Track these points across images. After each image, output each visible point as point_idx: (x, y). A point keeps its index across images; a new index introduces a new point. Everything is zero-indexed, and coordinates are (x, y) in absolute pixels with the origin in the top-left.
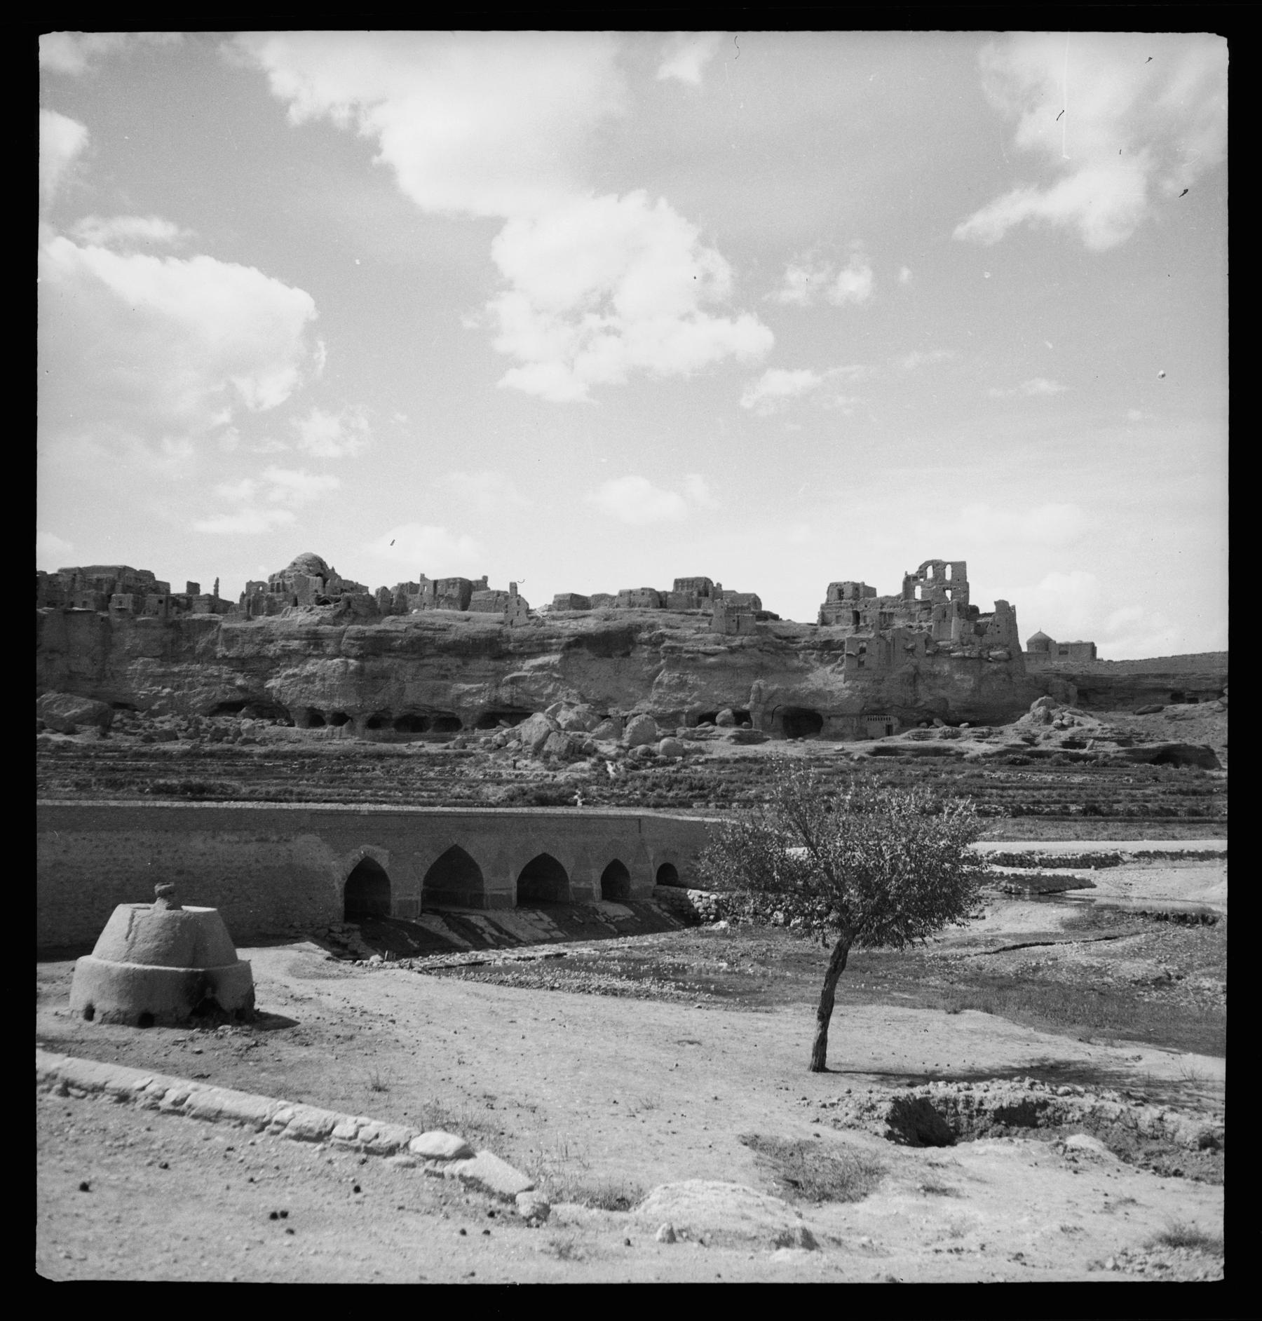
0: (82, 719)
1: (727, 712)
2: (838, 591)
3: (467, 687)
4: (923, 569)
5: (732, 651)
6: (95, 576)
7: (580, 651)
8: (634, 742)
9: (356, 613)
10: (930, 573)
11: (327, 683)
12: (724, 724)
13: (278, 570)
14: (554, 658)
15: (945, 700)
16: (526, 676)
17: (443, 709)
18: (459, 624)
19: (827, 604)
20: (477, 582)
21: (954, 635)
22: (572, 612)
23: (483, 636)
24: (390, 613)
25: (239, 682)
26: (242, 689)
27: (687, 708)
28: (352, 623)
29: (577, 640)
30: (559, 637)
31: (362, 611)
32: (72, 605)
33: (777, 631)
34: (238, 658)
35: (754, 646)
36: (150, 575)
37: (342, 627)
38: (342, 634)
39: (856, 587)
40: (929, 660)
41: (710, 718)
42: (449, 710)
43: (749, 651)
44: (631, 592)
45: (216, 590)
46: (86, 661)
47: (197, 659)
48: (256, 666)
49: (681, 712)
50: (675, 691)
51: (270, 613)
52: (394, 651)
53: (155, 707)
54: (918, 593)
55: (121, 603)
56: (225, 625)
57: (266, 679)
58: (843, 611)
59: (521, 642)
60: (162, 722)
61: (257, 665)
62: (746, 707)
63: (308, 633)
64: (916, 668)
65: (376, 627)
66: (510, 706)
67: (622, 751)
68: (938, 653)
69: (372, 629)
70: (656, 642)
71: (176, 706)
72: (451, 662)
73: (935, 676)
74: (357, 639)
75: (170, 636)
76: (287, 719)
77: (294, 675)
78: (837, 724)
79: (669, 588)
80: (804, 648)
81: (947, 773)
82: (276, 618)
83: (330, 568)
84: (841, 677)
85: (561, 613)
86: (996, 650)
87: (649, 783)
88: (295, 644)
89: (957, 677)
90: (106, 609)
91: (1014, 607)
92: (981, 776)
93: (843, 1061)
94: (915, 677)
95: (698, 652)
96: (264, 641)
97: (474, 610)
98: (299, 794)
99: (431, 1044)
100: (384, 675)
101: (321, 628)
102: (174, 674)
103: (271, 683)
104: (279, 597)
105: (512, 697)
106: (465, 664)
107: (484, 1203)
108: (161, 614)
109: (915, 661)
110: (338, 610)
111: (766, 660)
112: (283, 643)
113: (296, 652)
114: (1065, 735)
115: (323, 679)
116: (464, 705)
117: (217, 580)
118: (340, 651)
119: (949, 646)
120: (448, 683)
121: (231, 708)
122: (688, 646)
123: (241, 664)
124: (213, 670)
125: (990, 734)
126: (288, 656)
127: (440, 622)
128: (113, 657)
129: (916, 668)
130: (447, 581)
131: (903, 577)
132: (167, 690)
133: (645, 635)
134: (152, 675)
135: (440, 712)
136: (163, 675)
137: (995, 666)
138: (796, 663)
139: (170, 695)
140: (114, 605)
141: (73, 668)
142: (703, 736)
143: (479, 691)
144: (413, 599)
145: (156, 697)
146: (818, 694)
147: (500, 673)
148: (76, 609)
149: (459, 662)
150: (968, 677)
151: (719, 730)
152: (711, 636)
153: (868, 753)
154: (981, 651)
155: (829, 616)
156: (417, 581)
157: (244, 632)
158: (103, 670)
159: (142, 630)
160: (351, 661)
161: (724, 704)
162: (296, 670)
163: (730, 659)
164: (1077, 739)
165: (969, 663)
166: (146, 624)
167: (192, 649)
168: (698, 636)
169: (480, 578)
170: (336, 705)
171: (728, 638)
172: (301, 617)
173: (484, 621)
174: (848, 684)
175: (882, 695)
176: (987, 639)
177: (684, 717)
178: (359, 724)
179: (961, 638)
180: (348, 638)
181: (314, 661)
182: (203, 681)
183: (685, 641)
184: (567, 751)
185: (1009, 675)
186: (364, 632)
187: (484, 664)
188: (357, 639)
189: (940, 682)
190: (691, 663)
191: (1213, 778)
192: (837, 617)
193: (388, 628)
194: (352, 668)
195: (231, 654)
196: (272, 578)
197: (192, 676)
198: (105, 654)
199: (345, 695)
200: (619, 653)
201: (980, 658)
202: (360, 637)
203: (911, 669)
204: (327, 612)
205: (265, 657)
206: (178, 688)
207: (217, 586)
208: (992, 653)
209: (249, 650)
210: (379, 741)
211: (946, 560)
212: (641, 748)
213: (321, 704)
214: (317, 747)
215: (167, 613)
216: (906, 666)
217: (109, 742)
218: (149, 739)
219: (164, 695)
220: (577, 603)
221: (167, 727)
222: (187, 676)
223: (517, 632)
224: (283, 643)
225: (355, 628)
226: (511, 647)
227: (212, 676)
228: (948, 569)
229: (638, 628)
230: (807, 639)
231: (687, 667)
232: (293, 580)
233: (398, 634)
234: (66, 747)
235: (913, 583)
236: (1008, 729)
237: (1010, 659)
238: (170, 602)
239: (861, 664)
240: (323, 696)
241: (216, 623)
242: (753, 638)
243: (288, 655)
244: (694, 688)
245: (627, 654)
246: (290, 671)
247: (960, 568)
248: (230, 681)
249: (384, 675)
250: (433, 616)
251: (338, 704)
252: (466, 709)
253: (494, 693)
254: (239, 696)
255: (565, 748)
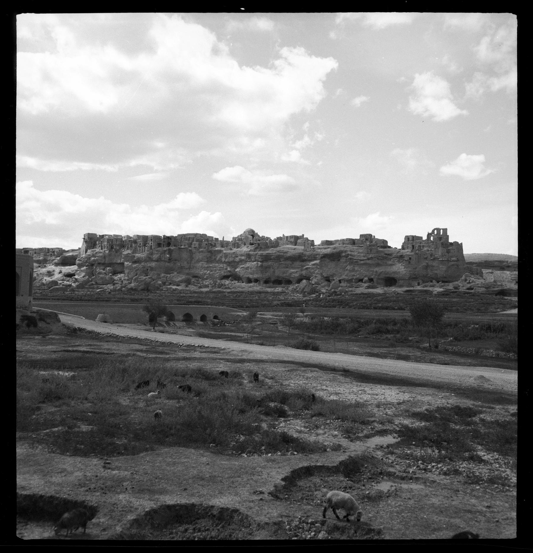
0: (181, 282)
1: (366, 279)
2: (407, 238)
3: (293, 271)
4: (433, 231)
5: (368, 259)
7: (325, 259)
8: (332, 289)
9: (261, 248)
10: (436, 232)
11: (252, 270)
12: (365, 282)
13: (239, 234)
14: (317, 262)
15: (436, 274)
16: (310, 267)
17: (287, 278)
20: (300, 236)
21: (440, 253)
22: (326, 246)
23: (297, 255)
25: (229, 269)
27: (355, 277)
28: (260, 251)
30: (319, 255)
31: (263, 247)
32: (181, 246)
33: (386, 252)
34: (228, 262)
35: (375, 258)
37: (257, 252)
41: (361, 280)
43: (374, 259)
44: (343, 240)
45: (223, 239)
46: (185, 263)
48: (233, 264)
49: (353, 279)
51: (238, 247)
52: (272, 259)
54: (432, 238)
55: (195, 245)
56: (224, 252)
57: (236, 268)
59: (309, 256)
60: (206, 282)
61: (234, 264)
62: (372, 277)
63: (247, 254)
66: (305, 276)
67: (328, 291)
68: (434, 259)
69: (265, 252)
70: (347, 256)
73: (433, 266)
74: (261, 256)
75: (209, 255)
76: (242, 281)
77: (243, 267)
78: (401, 282)
79: (358, 238)
80: (393, 258)
82: (239, 249)
84: (403, 267)
85: (322, 247)
87: (327, 301)
88: (243, 258)
89: (440, 267)
90: (190, 247)
94: (427, 267)
95: (358, 259)
98: (222, 303)
101: (250, 252)
102: (210, 267)
103: (237, 270)
104: (240, 243)
105: (306, 274)
107: (238, 393)
108: (207, 248)
109: (427, 261)
111: (379, 262)
112: (240, 257)
113: (243, 260)
114: (469, 285)
115: (251, 269)
117: (223, 237)
118: (256, 260)
120: (288, 269)
121: (226, 277)
122: (355, 258)
123: (229, 263)
124: (221, 266)
127: (285, 250)
128: (193, 262)
129: (427, 263)
130: (290, 236)
132: (208, 272)
133: (344, 254)
134: (205, 267)
136: (208, 267)
137: (453, 263)
138: (390, 262)
139: (209, 274)
140: (193, 246)
143: (297, 272)
144: (281, 242)
145: (205, 274)
146: (395, 273)
147: (303, 266)
149: (291, 263)
151: (363, 284)
152: (362, 254)
153: (403, 292)
156: (282, 236)
157: (229, 254)
160: (259, 263)
161: (366, 276)
162: (244, 266)
163: (368, 262)
164: (472, 287)
166: (202, 251)
167: (215, 259)
168: (359, 254)
172: (245, 249)
173: (300, 248)
174: (405, 269)
175: (416, 273)
176: (450, 254)
177: (354, 280)
178: (262, 282)
179: (442, 254)
180: (258, 256)
181: (248, 263)
182: (219, 269)
183: (355, 256)
186: (263, 254)
187: (298, 263)
188: (261, 256)
190: (356, 263)
191: (505, 299)
193: (270, 252)
194: (259, 265)
195: (226, 261)
198: (191, 260)
199: (257, 273)
202: (261, 255)
206: (212, 271)
208: (452, 259)
210: (267, 288)
211: (440, 228)
212: (333, 290)
213: (251, 276)
214: (251, 289)
216: (424, 263)
217: (188, 288)
218: (200, 287)
220: (328, 243)
221: (207, 283)
223: (308, 253)
224: (240, 257)
225: (260, 252)
227: (221, 267)
228: (441, 231)
229: (342, 252)
234: (176, 290)
235: (430, 236)
236: (451, 284)
239: (409, 262)
240: (251, 274)
243: (241, 261)
245: (339, 260)
246: (242, 266)
247: (445, 230)
248: (226, 269)
249: (268, 267)
250: (284, 248)
251: (256, 276)
252: (292, 278)
254: (229, 274)
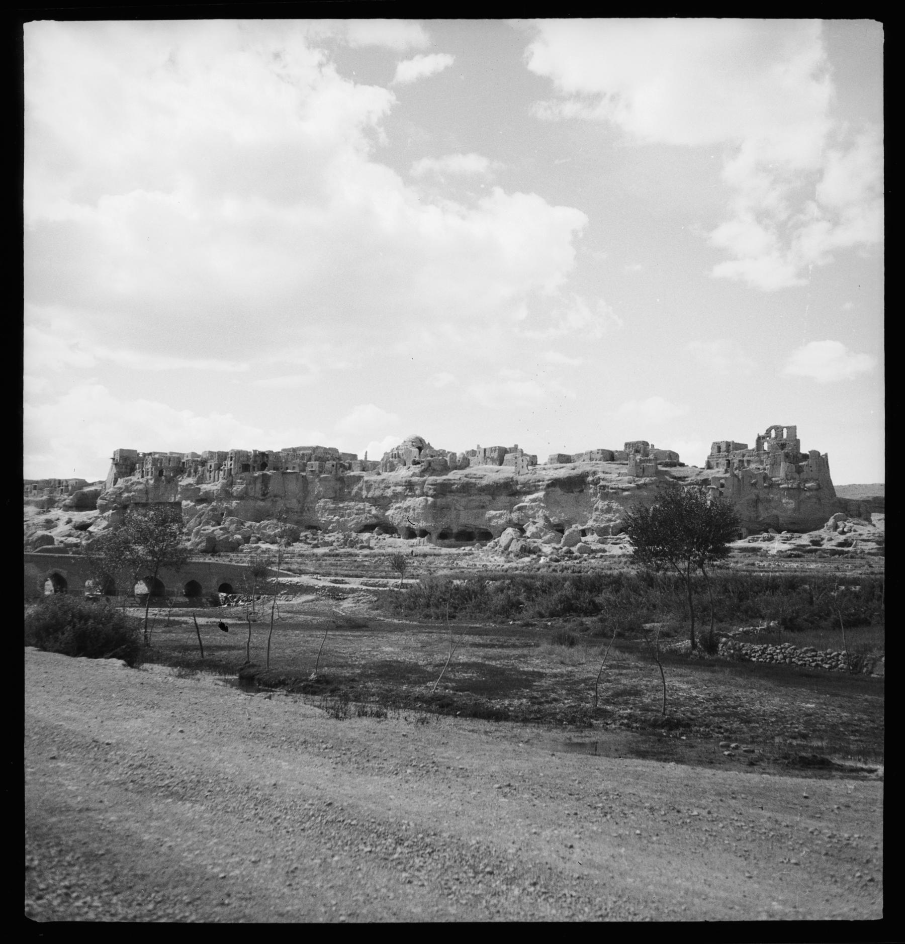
2: (718, 447)
4: (768, 432)
5: (639, 487)
6: (301, 452)
9: (434, 470)
11: (416, 511)
14: (541, 494)
15: (777, 517)
17: (482, 527)
18: (490, 474)
19: (711, 455)
22: (559, 465)
24: (456, 468)
25: (374, 512)
26: (376, 516)
27: (612, 524)
28: (431, 475)
29: (552, 483)
30: (543, 481)
34: (372, 498)
36: (336, 451)
37: (425, 478)
38: (424, 482)
39: (728, 444)
40: (766, 491)
42: (485, 527)
47: (352, 500)
48: (382, 502)
50: (605, 513)
53: (330, 528)
54: (766, 446)
56: (366, 479)
57: (387, 510)
58: (720, 460)
59: (525, 484)
61: (382, 502)
63: (406, 482)
64: (757, 496)
65: (444, 477)
69: (440, 479)
71: (341, 527)
72: (486, 498)
73: (769, 501)
75: (339, 485)
77: (399, 508)
81: (734, 562)
83: (427, 443)
86: (809, 483)
88: (399, 489)
90: (304, 470)
91: (826, 455)
92: (753, 564)
93: (506, 745)
94: (757, 501)
95: (619, 488)
96: (385, 487)
97: (506, 465)
99: (717, 735)
100: (447, 507)
102: (340, 508)
104: (396, 461)
105: (519, 519)
106: (494, 499)
109: (756, 491)
110: (423, 468)
114: (842, 538)
115: (414, 510)
116: (492, 524)
117: (366, 453)
119: (778, 481)
121: (369, 528)
123: (375, 501)
124: (361, 505)
125: (791, 538)
126: (396, 496)
129: (757, 496)
131: (756, 437)
132: (337, 517)
133: (590, 479)
134: (329, 509)
135: (480, 529)
136: (335, 509)
137: (808, 494)
140: (308, 469)
141: (288, 506)
142: (618, 541)
144: (473, 460)
145: (330, 522)
148: (288, 471)
150: (791, 501)
152: (626, 478)
154: (799, 483)
155: (712, 463)
158: (303, 506)
159: (324, 482)
165: (792, 491)
168: (619, 478)
169: (513, 446)
170: (421, 525)
171: (637, 479)
176: (804, 476)
178: (434, 537)
179: (786, 475)
181: (409, 499)
182: (355, 511)
183: (611, 481)
184: (520, 550)
185: (819, 500)
187: (503, 499)
189: (773, 504)
190: (614, 495)
192: (717, 464)
194: (429, 502)
196: (392, 451)
197: (350, 509)
198: (305, 497)
200: (577, 490)
201: (798, 488)
203: (754, 497)
204: (417, 469)
205: (386, 497)
206: (342, 516)
207: (366, 456)
208: (807, 485)
209: (378, 493)
211: (783, 425)
215: (337, 472)
219: (334, 520)
222: (346, 510)
225: (431, 479)
226: (518, 487)
227: (360, 509)
228: (785, 431)
230: (693, 478)
231: (612, 499)
232: (403, 451)
233: (456, 482)
235: (762, 441)
237: (820, 488)
238: (338, 466)
241: (363, 477)
242: (653, 479)
244: (617, 511)
245: (582, 491)
246: (398, 505)
247: (792, 430)
249: (447, 507)
251: (422, 524)
253: (508, 517)
254: (374, 521)
255: (519, 548)
